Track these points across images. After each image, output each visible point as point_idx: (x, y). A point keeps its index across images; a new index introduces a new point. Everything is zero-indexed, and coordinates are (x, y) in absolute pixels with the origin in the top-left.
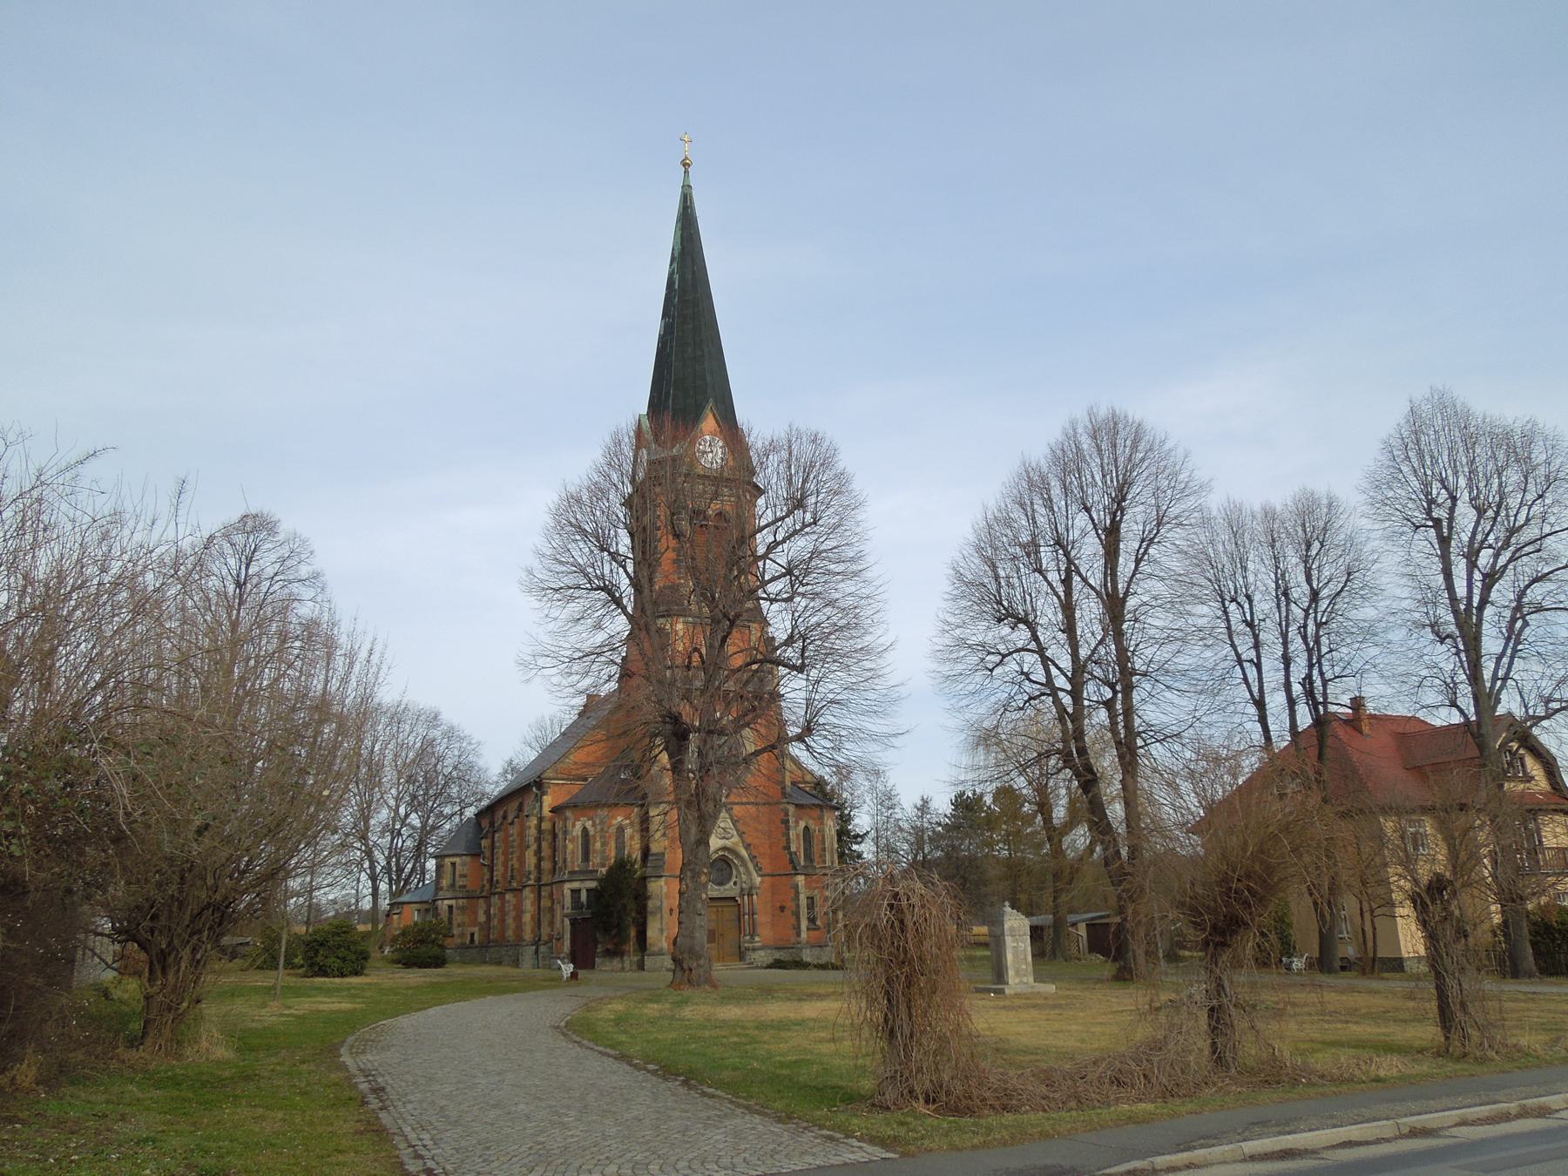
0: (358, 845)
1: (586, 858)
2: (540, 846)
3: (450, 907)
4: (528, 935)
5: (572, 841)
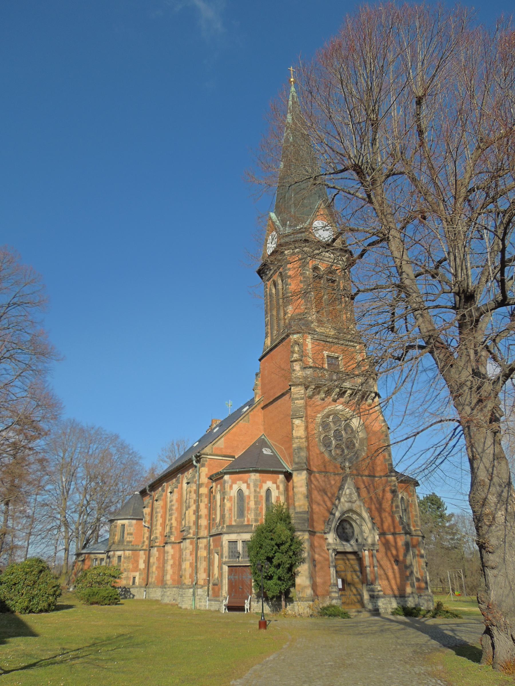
0: (59, 516)
1: (241, 513)
2: (198, 507)
3: (120, 557)
5: (230, 499)
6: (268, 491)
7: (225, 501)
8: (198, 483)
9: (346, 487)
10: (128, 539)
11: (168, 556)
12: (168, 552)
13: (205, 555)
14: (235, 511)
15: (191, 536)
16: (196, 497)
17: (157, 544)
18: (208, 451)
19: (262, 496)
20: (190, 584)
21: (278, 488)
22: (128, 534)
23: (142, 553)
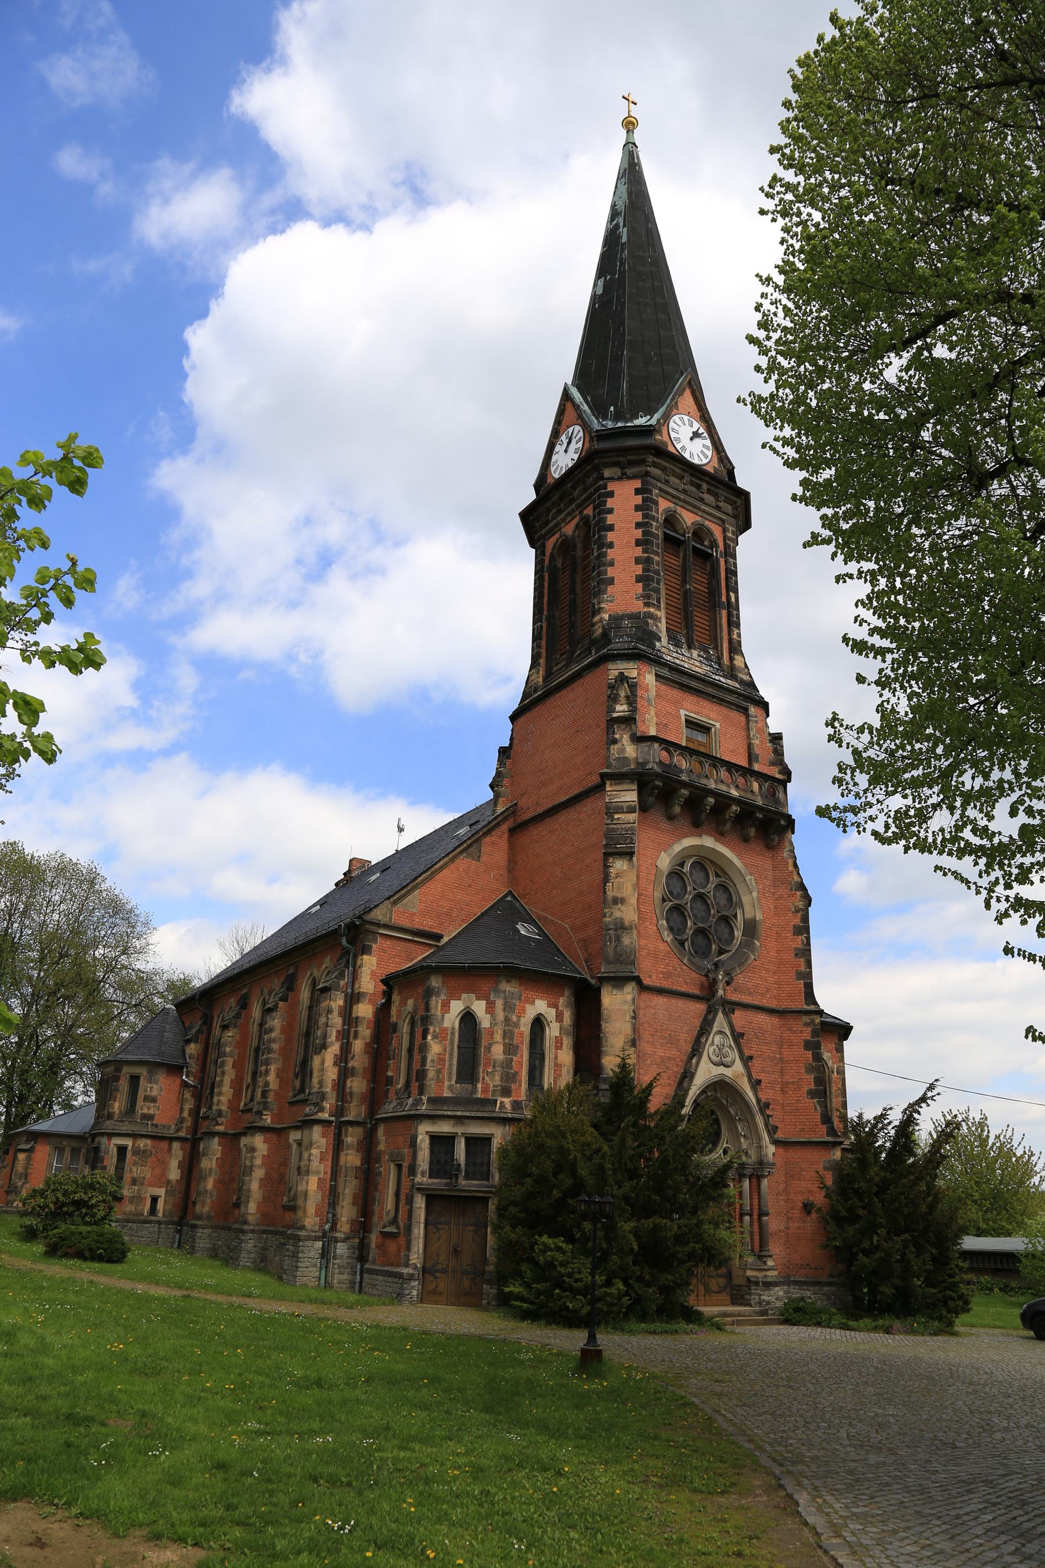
4: (310, 1219)
6: (538, 1023)
7: (429, 1037)
8: (349, 990)
9: (715, 1029)
10: (145, 1111)
13: (358, 1162)
14: (451, 1065)
15: (325, 1116)
16: (344, 1024)
17: (221, 1128)
18: (380, 917)
19: (522, 1034)
20: (317, 1228)
21: (559, 1017)
23: (176, 1145)
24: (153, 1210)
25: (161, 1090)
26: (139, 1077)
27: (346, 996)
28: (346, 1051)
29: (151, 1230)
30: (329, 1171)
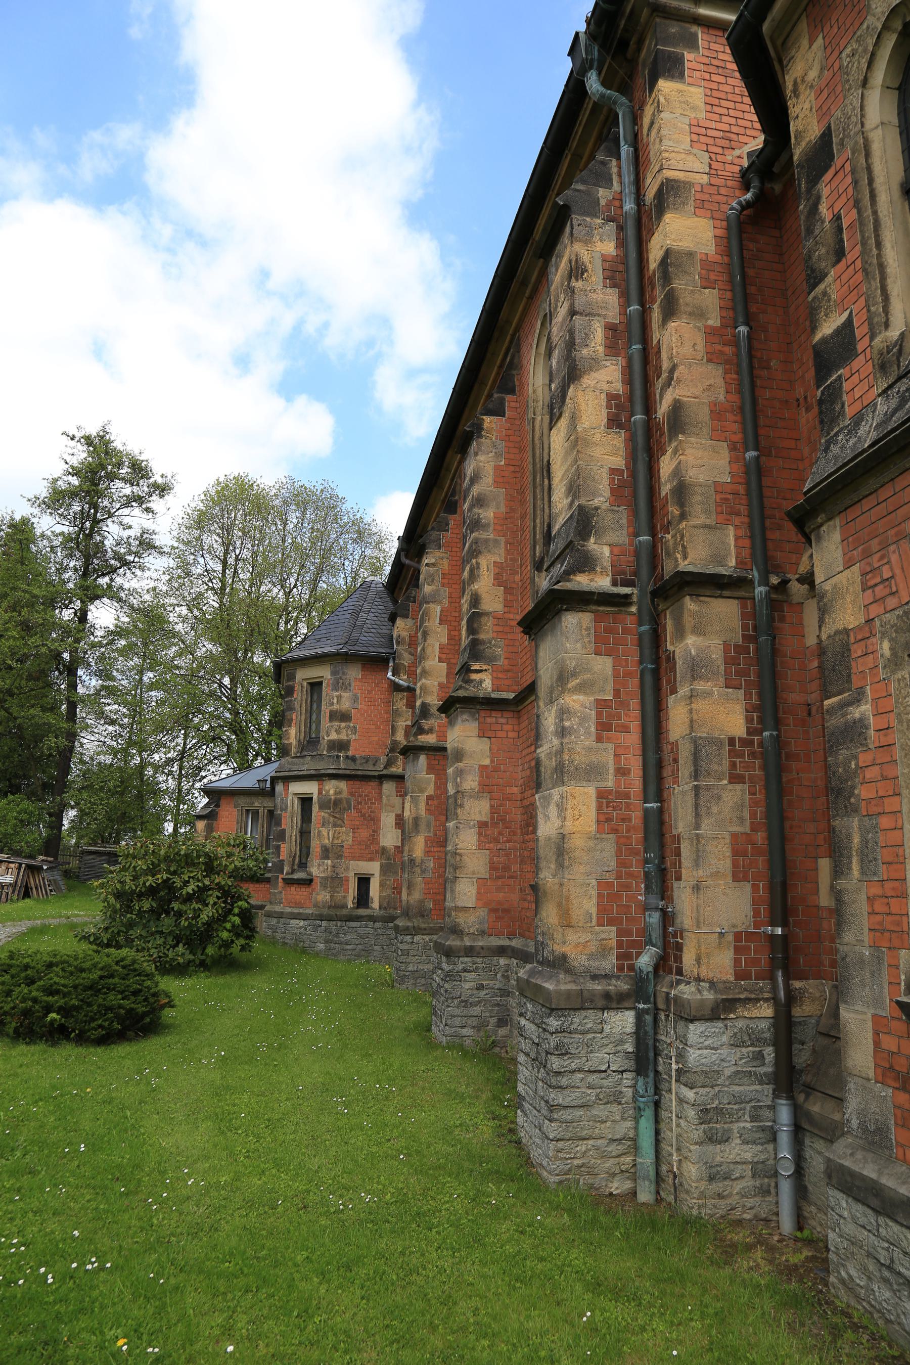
10: (334, 736)
11: (460, 773)
12: (459, 755)
20: (609, 963)
22: (333, 716)
24: (363, 899)
25: (355, 699)
26: (321, 683)
27: (621, 228)
28: (645, 370)
29: (361, 931)
30: (635, 764)
